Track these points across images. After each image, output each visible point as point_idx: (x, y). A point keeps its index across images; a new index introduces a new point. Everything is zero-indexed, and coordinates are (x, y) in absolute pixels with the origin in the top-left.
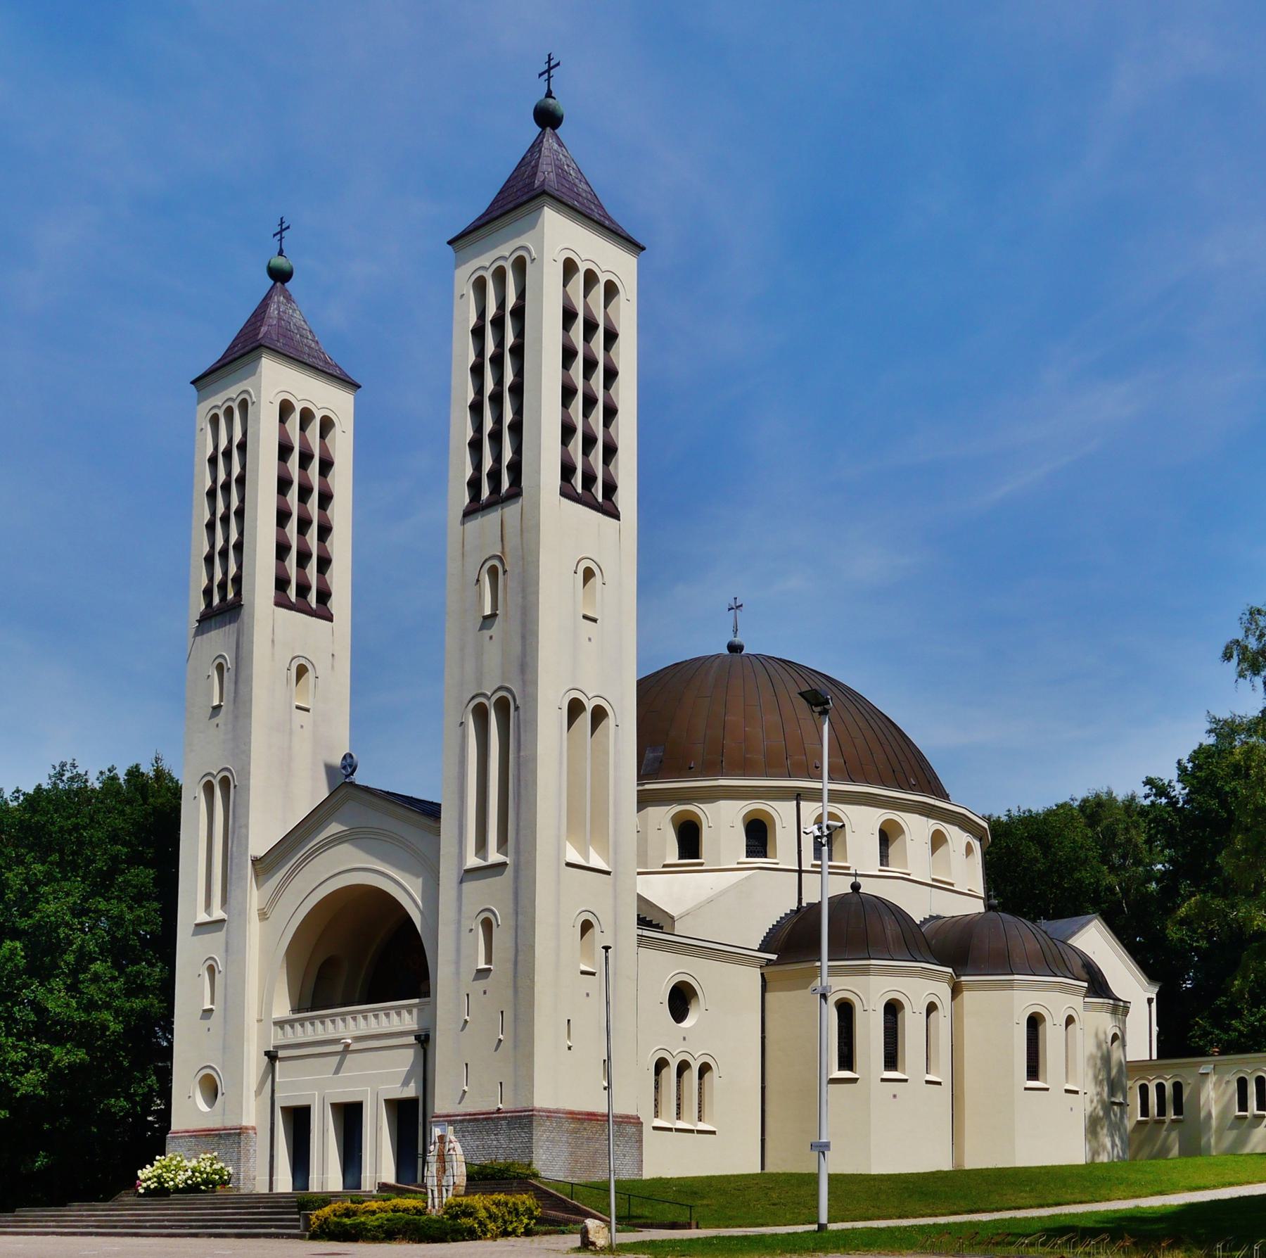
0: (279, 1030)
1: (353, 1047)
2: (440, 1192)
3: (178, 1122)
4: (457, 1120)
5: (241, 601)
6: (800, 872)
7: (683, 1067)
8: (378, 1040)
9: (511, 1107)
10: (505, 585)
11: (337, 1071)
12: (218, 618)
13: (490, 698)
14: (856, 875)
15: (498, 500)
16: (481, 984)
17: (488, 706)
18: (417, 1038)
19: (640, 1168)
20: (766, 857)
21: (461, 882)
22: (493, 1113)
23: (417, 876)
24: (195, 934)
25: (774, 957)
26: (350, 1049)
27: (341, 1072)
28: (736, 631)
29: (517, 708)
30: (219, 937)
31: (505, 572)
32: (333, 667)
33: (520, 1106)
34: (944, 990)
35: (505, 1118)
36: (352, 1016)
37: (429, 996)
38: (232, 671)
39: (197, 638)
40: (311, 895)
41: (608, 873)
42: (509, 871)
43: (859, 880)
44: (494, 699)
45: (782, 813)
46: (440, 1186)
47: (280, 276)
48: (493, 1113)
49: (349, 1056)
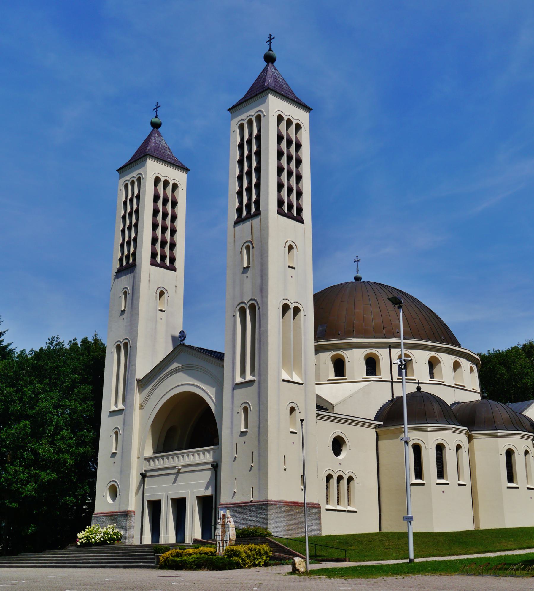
1: (183, 470)
2: (223, 543)
3: (99, 508)
6: (392, 382)
7: (340, 478)
14: (419, 383)
15: (250, 216)
16: (243, 439)
18: (212, 465)
19: (320, 531)
20: (376, 375)
21: (233, 390)
22: (248, 503)
23: (214, 387)
24: (109, 416)
25: (381, 423)
26: (181, 471)
28: (358, 271)
29: (259, 308)
30: (121, 417)
32: (176, 292)
37: (218, 445)
38: (131, 295)
40: (162, 398)
41: (302, 384)
43: (420, 385)
44: (248, 304)
45: (382, 354)
46: (223, 540)
47: (156, 126)
49: (180, 475)
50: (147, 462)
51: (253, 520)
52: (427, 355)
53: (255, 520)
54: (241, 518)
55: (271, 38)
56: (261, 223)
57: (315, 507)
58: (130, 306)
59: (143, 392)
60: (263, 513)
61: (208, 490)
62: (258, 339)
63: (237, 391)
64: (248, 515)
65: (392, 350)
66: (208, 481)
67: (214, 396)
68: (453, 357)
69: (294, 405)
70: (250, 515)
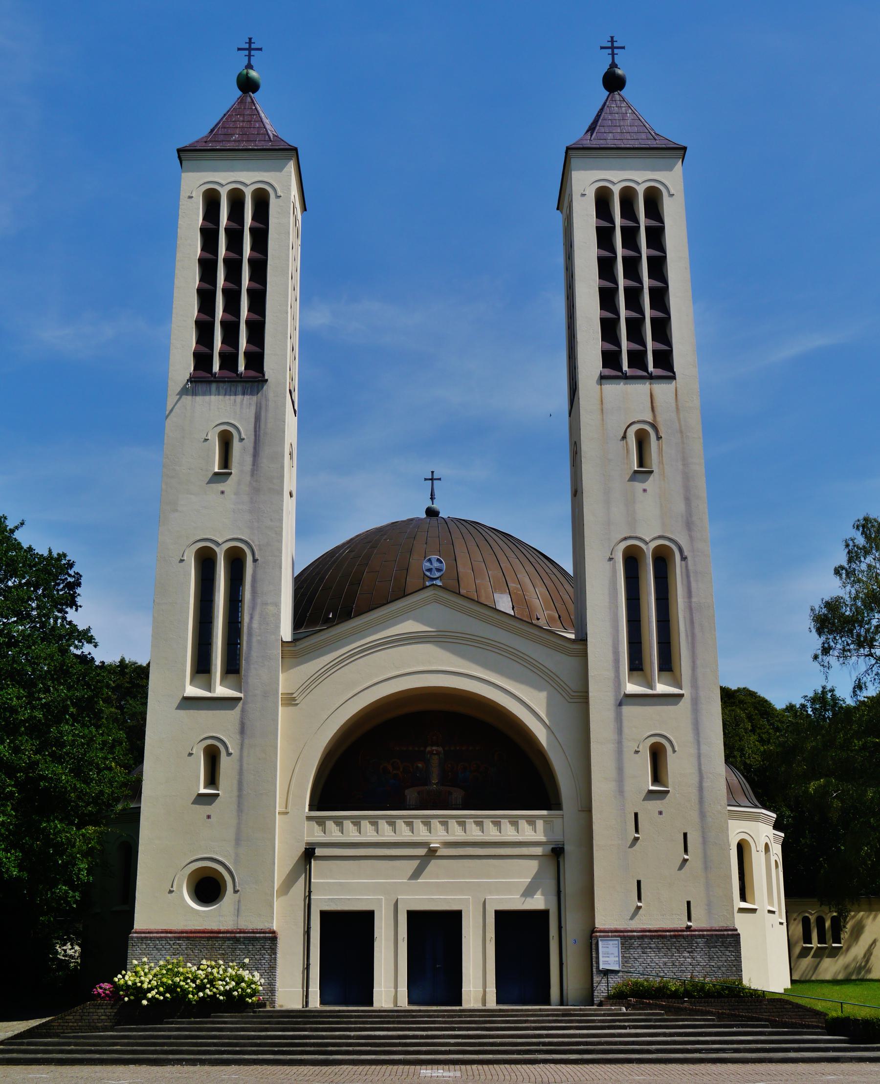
0: (316, 826)
1: (442, 852)
4: (634, 936)
5: (264, 375)
8: (482, 848)
9: (705, 926)
10: (660, 450)
12: (226, 385)
13: (648, 543)
16: (655, 805)
17: (645, 550)
22: (683, 931)
23: (540, 689)
26: (437, 854)
27: (528, 883)
28: (432, 498)
29: (684, 558)
30: (232, 716)
31: (659, 438)
33: (716, 925)
35: (703, 936)
36: (439, 820)
39: (184, 397)
40: (366, 691)
44: (653, 545)
47: (248, 85)
48: (683, 931)
49: (434, 863)
50: (315, 824)
51: (701, 964)
53: (705, 964)
54: (664, 960)
56: (679, 397)
58: (248, 467)
59: (298, 668)
60: (728, 952)
61: (534, 899)
62: (685, 617)
63: (626, 710)
64: (684, 955)
66: (530, 880)
67: (545, 712)
70: (691, 954)
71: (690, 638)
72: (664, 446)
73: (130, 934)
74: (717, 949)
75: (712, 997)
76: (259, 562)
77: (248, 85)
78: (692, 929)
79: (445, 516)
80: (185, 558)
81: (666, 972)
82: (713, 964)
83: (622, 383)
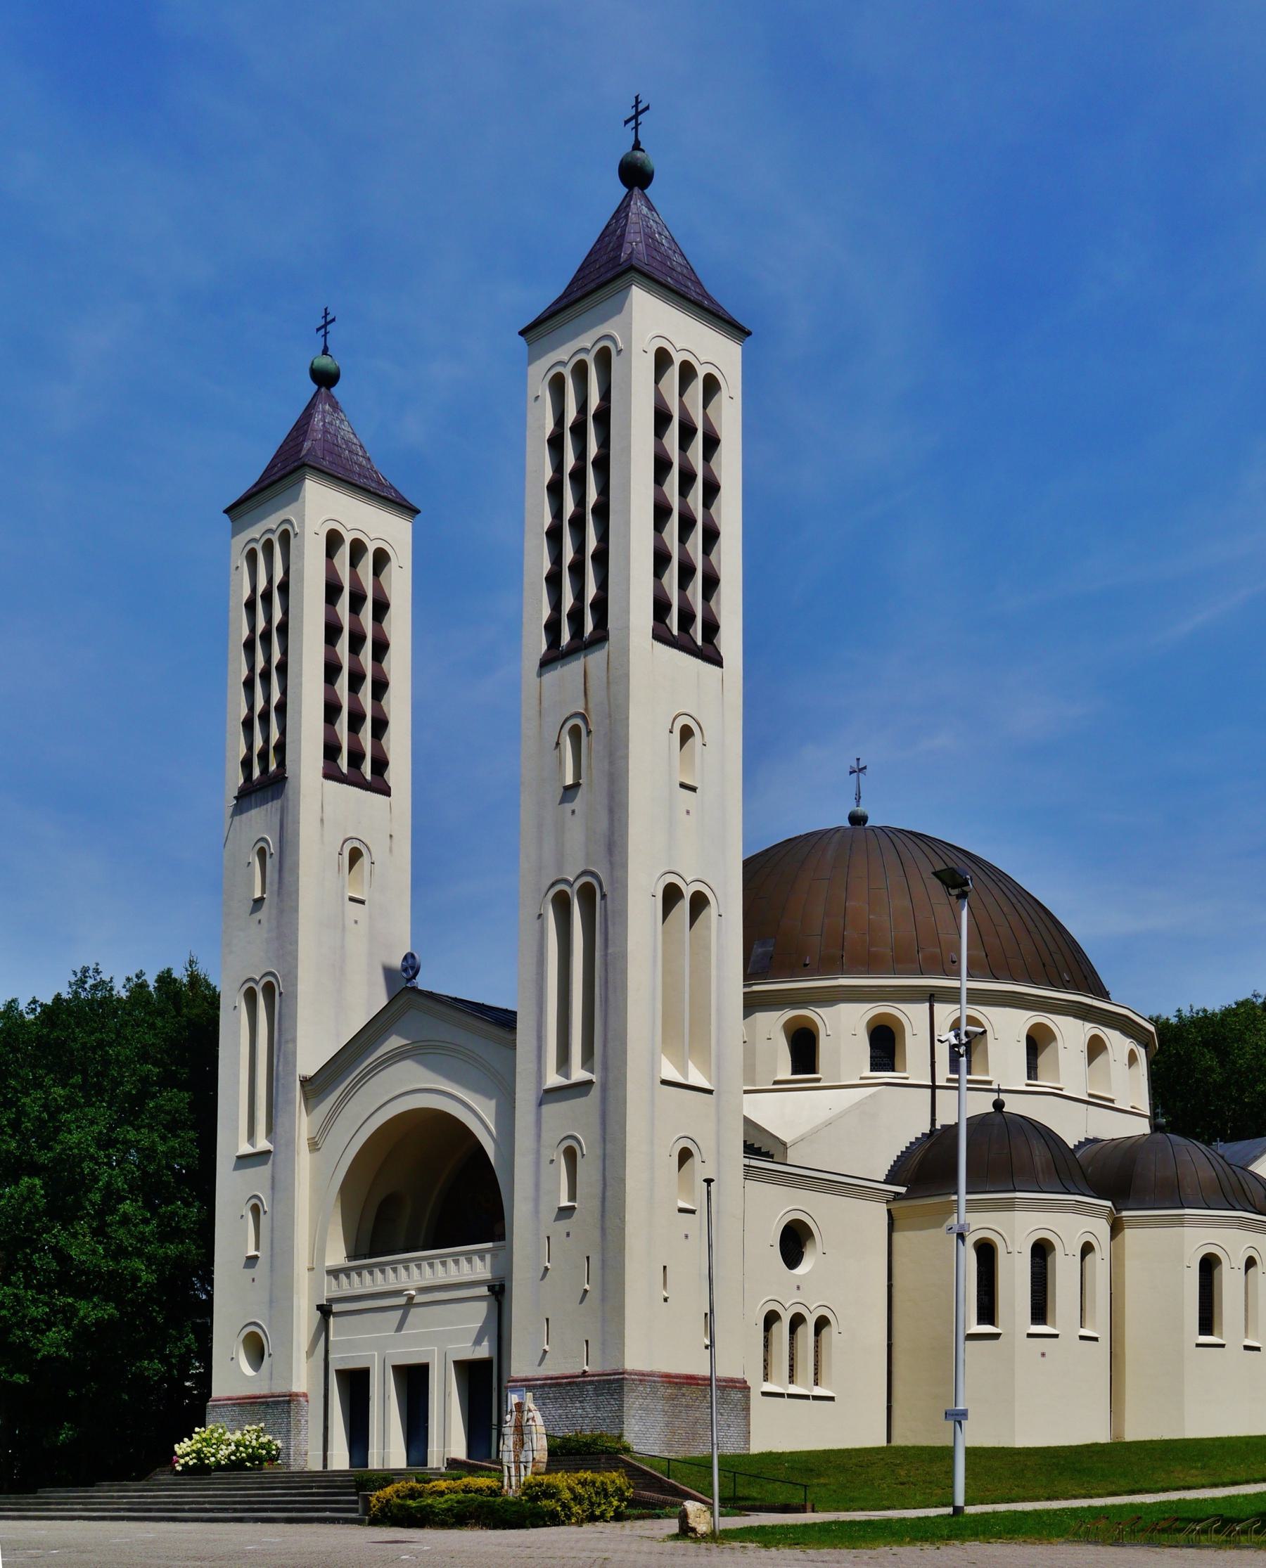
1: (418, 1300)
2: (518, 1469)
3: (221, 1387)
6: (933, 1088)
7: (798, 1320)
9: (599, 1370)
11: (400, 1328)
15: (581, 646)
16: (564, 1225)
19: (747, 1441)
21: (540, 1104)
22: (578, 1377)
23: (491, 1099)
24: (236, 1168)
25: (903, 1190)
26: (414, 1302)
29: (604, 896)
32: (391, 850)
34: (1101, 1228)
35: (591, 1382)
37: (504, 1239)
38: (276, 857)
40: (370, 1120)
41: (710, 1092)
42: (595, 1092)
43: (1003, 1096)
44: (577, 886)
46: (517, 1462)
47: (325, 379)
49: (413, 1311)
51: (590, 1416)
52: (1023, 1020)
53: (592, 1415)
54: (559, 1411)
55: (641, 107)
57: (736, 1387)
58: (276, 887)
65: (937, 1006)
68: (1089, 1025)
69: (689, 1144)
71: (603, 1002)
72: (593, 742)
73: (208, 1402)
74: (603, 1398)
75: (578, 1453)
76: (283, 994)
77: (325, 379)
78: (587, 1374)
79: (74, 982)
80: (237, 1005)
81: (560, 1426)
82: (600, 1415)
83: (559, 667)
